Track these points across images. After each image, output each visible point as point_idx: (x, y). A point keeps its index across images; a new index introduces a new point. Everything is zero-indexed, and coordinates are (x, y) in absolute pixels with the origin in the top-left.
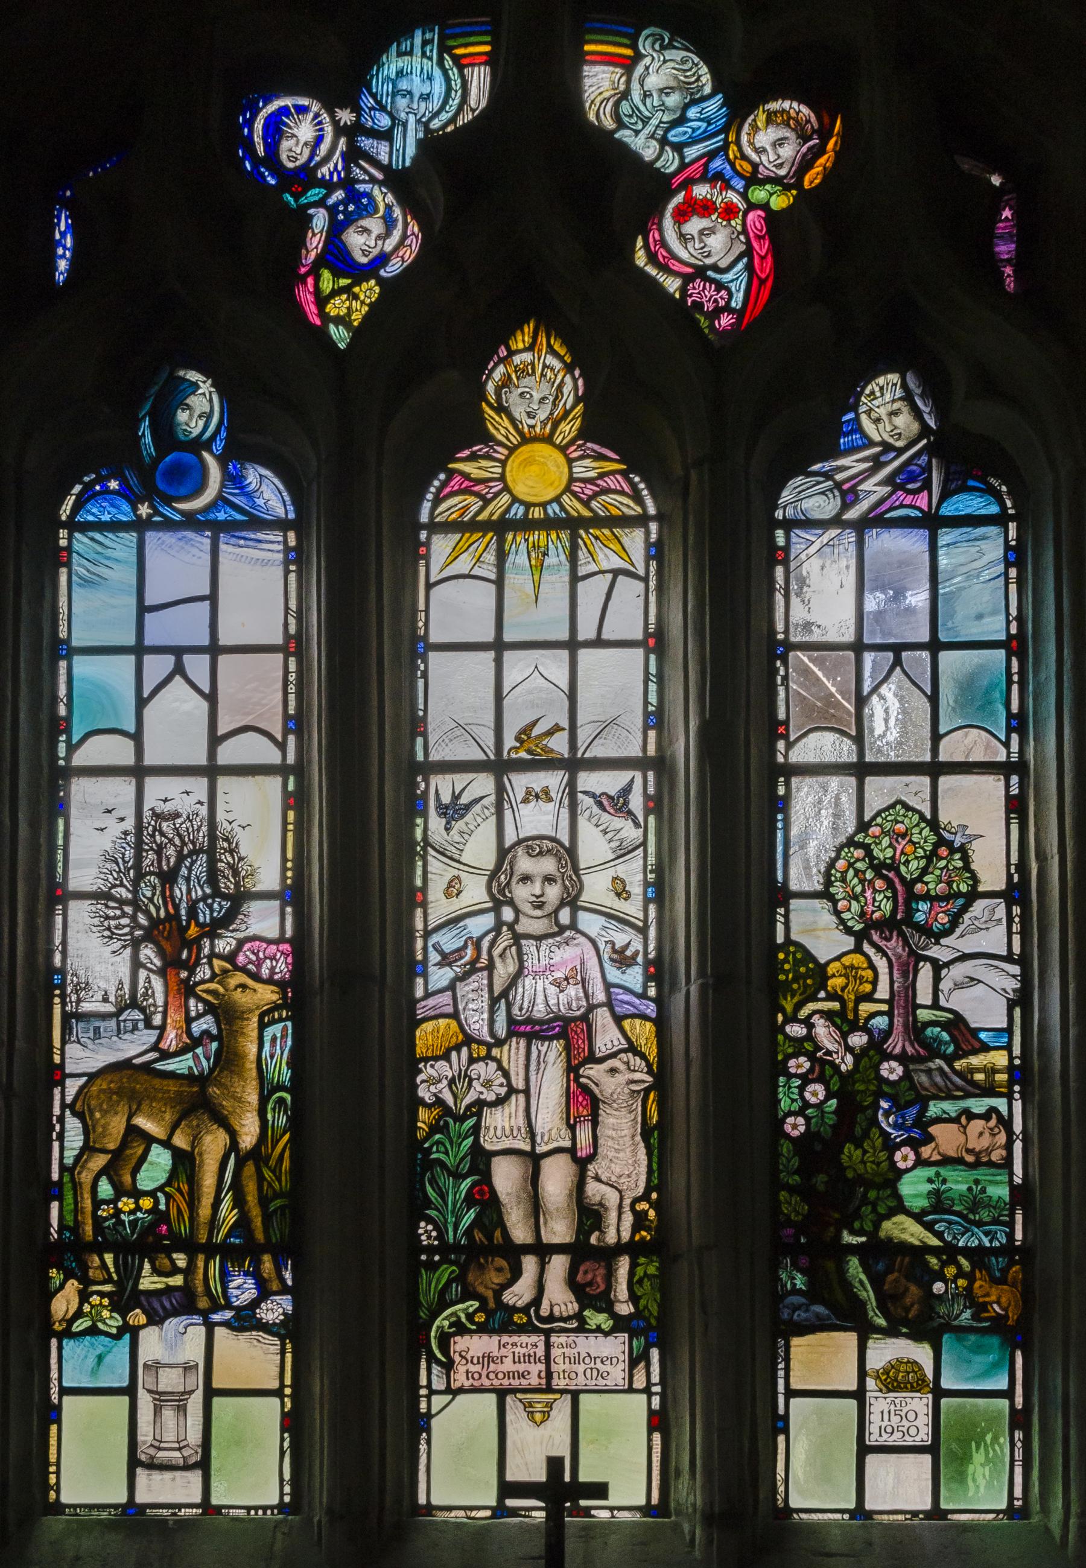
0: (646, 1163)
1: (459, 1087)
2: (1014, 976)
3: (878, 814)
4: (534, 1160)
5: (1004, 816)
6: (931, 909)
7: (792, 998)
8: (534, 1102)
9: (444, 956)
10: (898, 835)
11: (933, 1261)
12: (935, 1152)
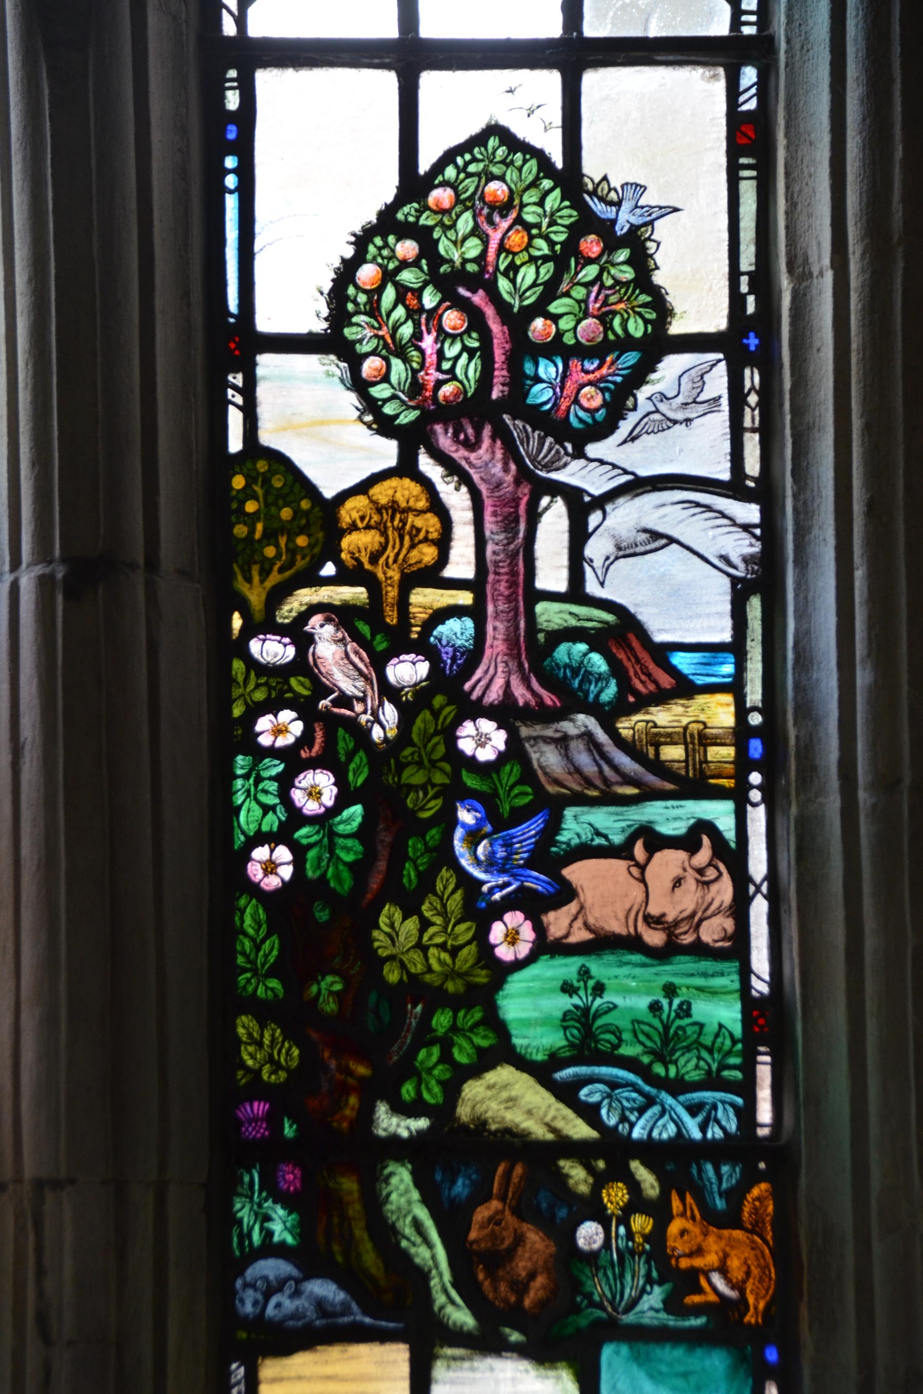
2: (746, 528)
3: (449, 157)
5: (723, 161)
6: (565, 377)
7: (262, 582)
10: (492, 207)
11: (577, 1175)
12: (579, 923)
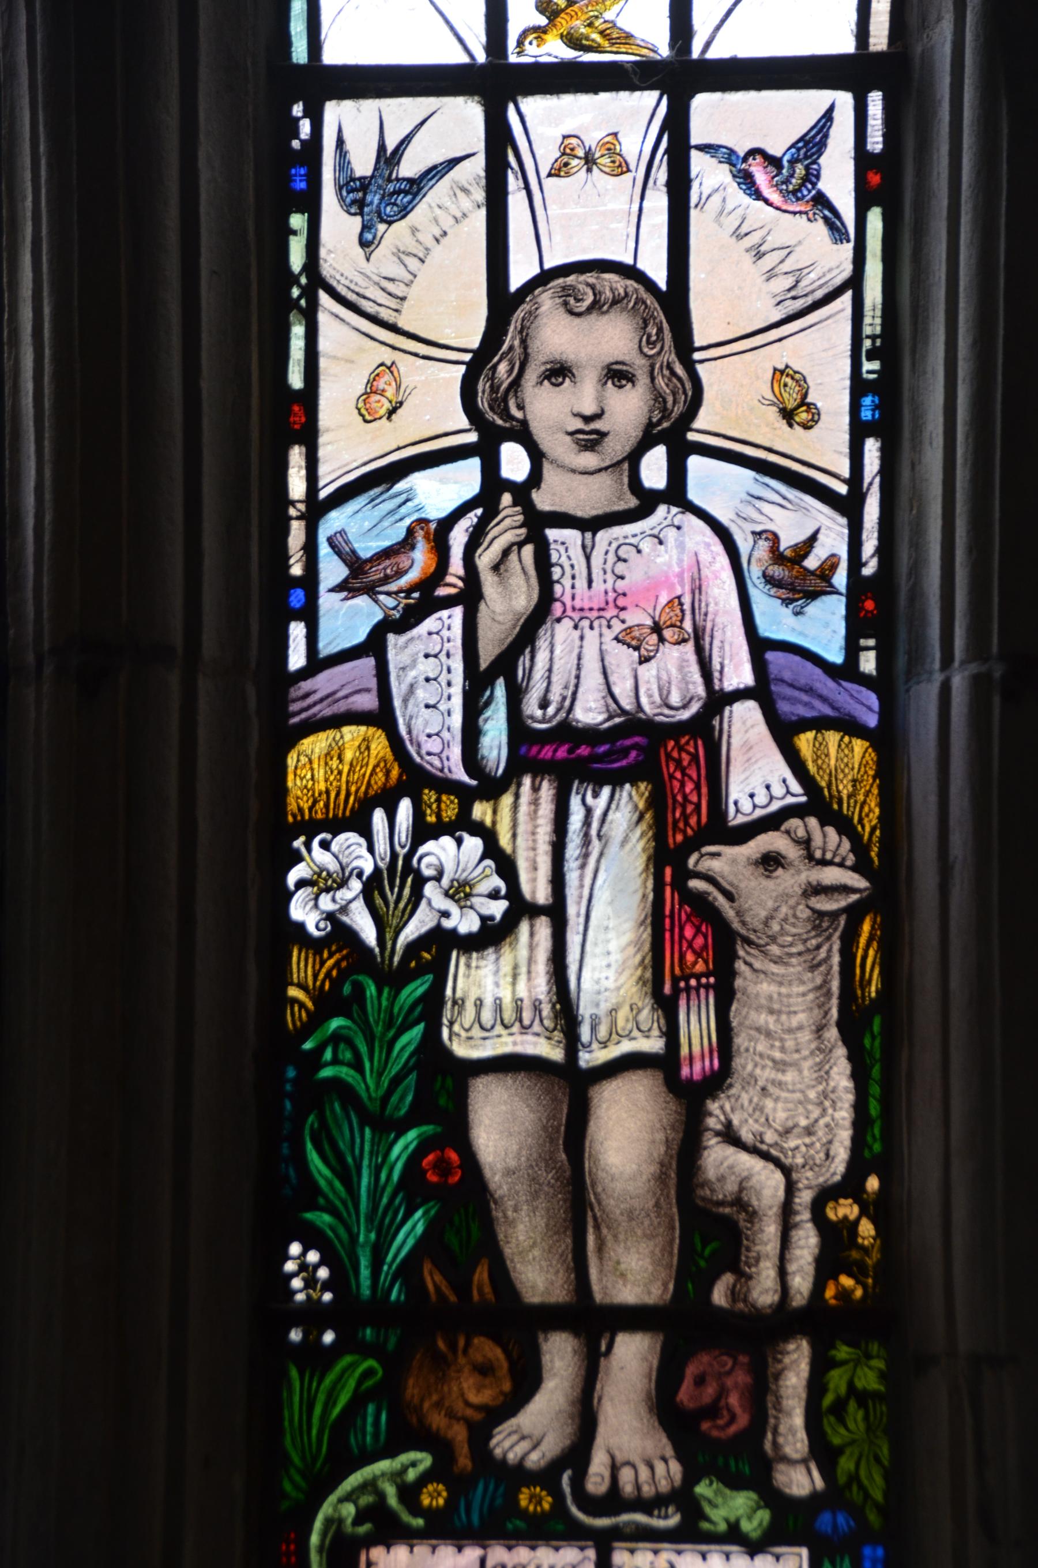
0: (850, 1097)
1: (392, 898)
4: (569, 1088)
8: (573, 940)
9: (356, 565)
